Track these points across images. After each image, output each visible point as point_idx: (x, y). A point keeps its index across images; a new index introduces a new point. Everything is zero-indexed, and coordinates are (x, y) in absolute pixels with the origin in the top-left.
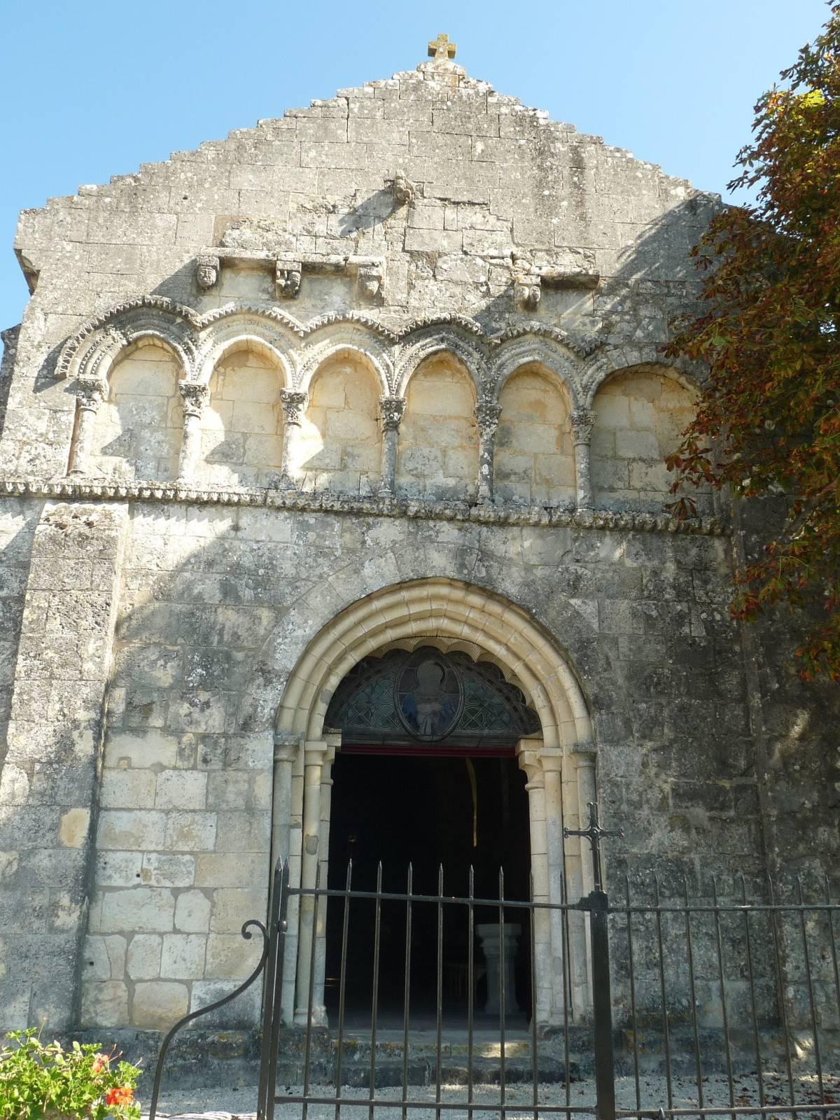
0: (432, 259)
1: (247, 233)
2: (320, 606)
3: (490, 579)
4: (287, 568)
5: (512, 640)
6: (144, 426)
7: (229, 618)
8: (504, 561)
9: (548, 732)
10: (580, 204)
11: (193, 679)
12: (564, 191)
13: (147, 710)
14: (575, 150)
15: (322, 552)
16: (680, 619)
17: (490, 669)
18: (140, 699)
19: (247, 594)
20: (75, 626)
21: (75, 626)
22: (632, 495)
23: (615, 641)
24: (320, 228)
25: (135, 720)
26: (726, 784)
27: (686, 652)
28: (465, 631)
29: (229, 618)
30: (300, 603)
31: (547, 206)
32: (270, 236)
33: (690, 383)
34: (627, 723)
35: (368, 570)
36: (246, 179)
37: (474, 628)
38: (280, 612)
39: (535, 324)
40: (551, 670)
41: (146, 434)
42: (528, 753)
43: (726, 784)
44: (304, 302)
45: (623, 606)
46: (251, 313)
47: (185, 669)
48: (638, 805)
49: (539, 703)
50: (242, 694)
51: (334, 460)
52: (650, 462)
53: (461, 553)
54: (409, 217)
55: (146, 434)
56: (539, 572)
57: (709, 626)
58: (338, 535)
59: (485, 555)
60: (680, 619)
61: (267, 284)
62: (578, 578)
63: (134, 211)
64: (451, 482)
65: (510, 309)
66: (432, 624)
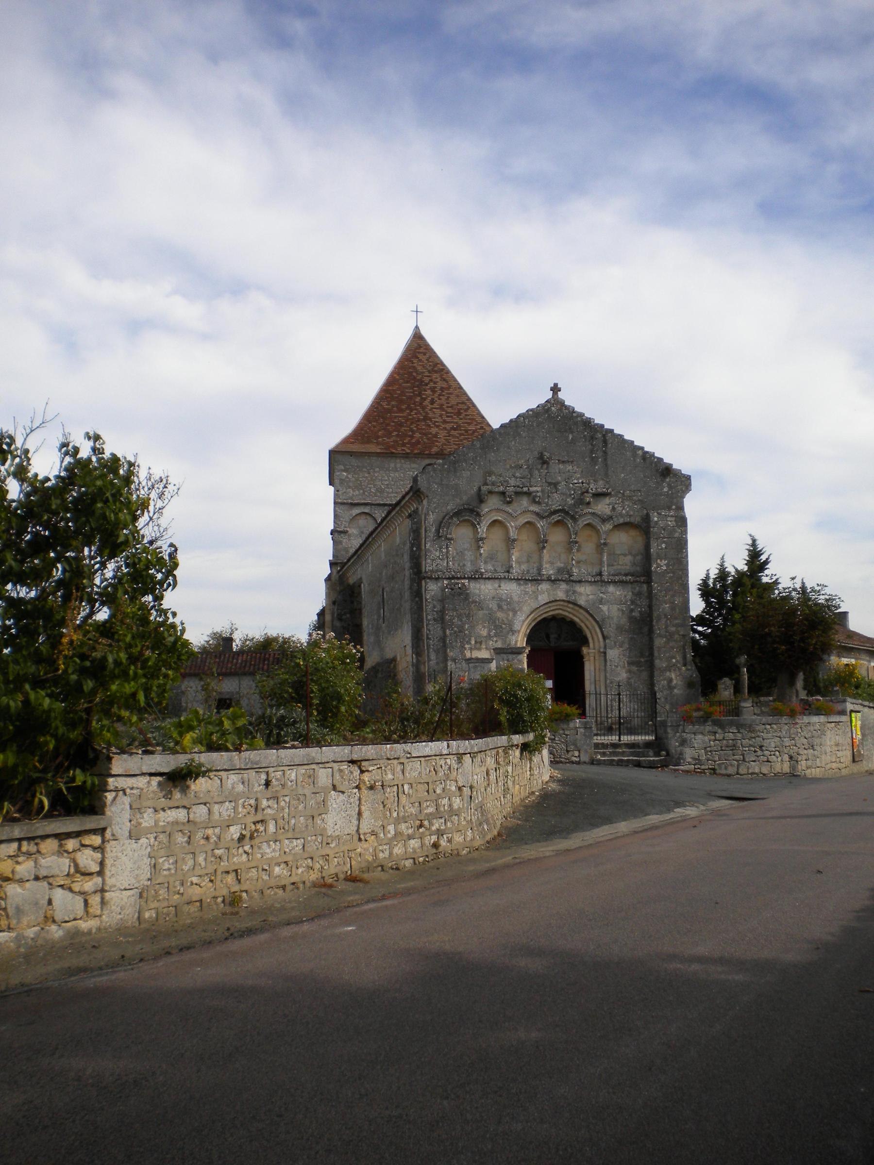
0: (555, 485)
1: (494, 478)
2: (526, 609)
3: (575, 600)
4: (516, 599)
5: (581, 617)
6: (465, 550)
7: (500, 615)
8: (580, 594)
9: (591, 645)
10: (605, 460)
11: (492, 634)
12: (600, 454)
13: (481, 643)
14: (604, 436)
15: (526, 593)
16: (632, 611)
17: (572, 623)
18: (478, 640)
19: (505, 607)
20: (461, 621)
21: (461, 621)
22: (619, 567)
23: (612, 618)
24: (518, 474)
25: (478, 646)
26: (642, 660)
27: (632, 619)
28: (567, 614)
29: (500, 615)
30: (520, 609)
31: (594, 461)
32: (502, 479)
33: (669, 810)
34: (615, 643)
35: (540, 598)
36: (492, 456)
37: (569, 612)
38: (515, 612)
39: (590, 510)
40: (593, 627)
41: (466, 552)
42: (585, 650)
43: (642, 660)
44: (515, 505)
45: (615, 607)
46: (498, 510)
47: (490, 631)
48: (617, 667)
49: (589, 636)
50: (506, 637)
51: (524, 559)
52: (625, 555)
53: (567, 592)
54: (547, 468)
55: (466, 552)
56: (591, 597)
57: (640, 612)
58: (530, 588)
59: (574, 592)
60: (632, 611)
61: (502, 498)
62: (602, 598)
63: (455, 471)
64: (562, 565)
65: (581, 504)
66: (557, 612)
